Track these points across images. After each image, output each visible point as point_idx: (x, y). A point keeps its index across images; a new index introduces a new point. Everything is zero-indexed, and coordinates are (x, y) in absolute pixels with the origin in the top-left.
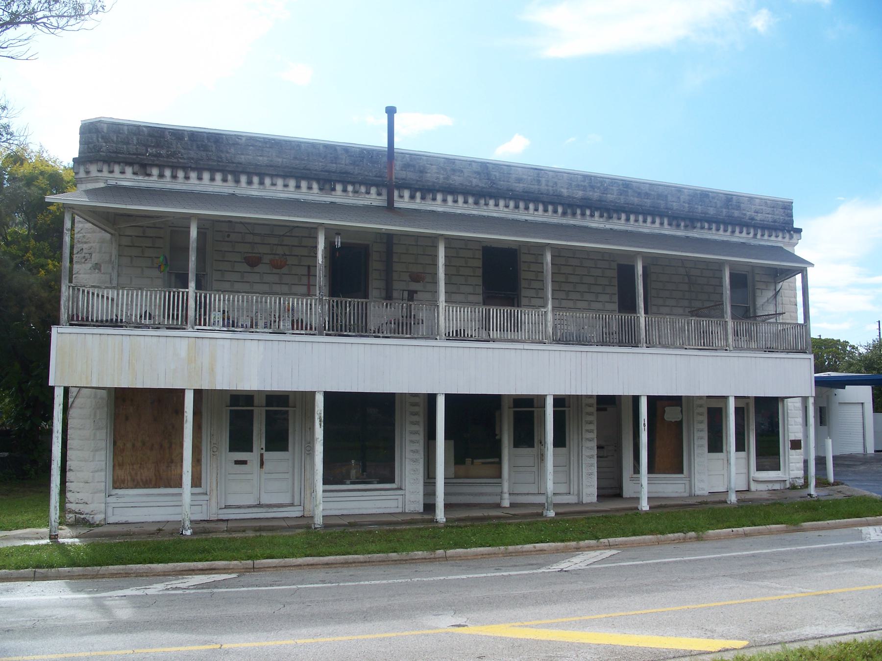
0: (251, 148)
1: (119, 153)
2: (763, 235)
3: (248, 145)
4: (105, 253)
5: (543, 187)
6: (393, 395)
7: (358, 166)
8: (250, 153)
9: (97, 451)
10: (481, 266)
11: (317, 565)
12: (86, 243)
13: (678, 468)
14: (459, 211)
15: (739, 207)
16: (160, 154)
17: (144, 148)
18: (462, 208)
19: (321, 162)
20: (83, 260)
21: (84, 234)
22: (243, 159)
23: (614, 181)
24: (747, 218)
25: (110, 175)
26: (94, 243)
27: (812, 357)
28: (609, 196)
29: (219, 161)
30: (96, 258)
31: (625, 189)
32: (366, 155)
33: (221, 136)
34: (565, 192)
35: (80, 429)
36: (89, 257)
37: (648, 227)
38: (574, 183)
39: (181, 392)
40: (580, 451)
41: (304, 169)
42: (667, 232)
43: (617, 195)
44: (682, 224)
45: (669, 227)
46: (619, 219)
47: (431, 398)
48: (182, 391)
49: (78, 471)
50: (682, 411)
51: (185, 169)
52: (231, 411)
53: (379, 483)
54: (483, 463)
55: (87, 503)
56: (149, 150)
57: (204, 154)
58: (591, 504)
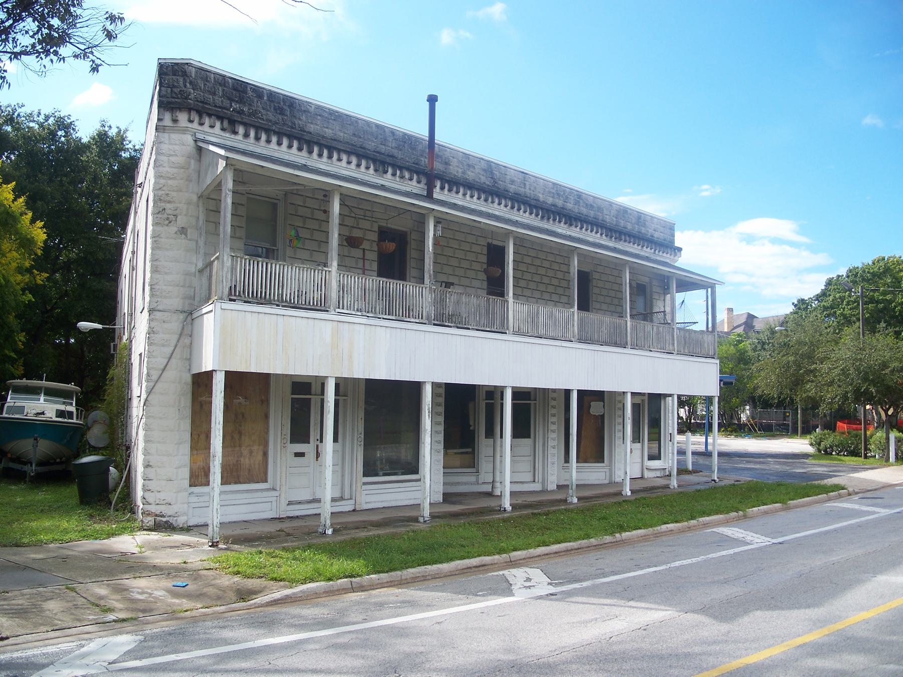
0: (319, 117)
1: (206, 103)
3: (317, 114)
4: (191, 216)
6: (475, 385)
7: (401, 150)
8: (319, 123)
9: (180, 443)
10: (486, 262)
11: (550, 554)
12: (169, 202)
13: (600, 458)
15: (645, 224)
16: (242, 110)
17: (229, 102)
18: (476, 204)
19: (374, 142)
20: (167, 222)
21: (167, 192)
22: (312, 128)
25: (200, 128)
26: (180, 203)
27: (718, 362)
28: (568, 204)
29: (292, 128)
30: (182, 221)
32: (407, 141)
33: (294, 100)
34: (541, 197)
35: (161, 418)
36: (174, 219)
37: (593, 237)
38: (547, 190)
40: (546, 442)
41: (361, 147)
47: (568, 392)
49: (159, 467)
50: (604, 406)
51: (268, 131)
52: (486, 403)
53: (403, 474)
54: (456, 453)
55: (170, 504)
56: (233, 104)
57: (280, 117)
58: (552, 491)
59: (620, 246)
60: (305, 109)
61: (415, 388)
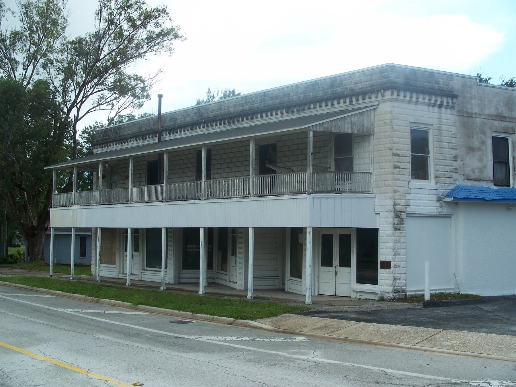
2: (357, 100)
5: (223, 111)
14: (187, 136)
23: (258, 95)
24: (348, 90)
31: (264, 98)
39: (247, 229)
42: (287, 118)
43: (260, 103)
44: (295, 110)
45: (287, 115)
46: (257, 118)
48: (248, 228)
52: (134, 235)
59: (126, 146)
60: (122, 128)
61: (161, 229)
